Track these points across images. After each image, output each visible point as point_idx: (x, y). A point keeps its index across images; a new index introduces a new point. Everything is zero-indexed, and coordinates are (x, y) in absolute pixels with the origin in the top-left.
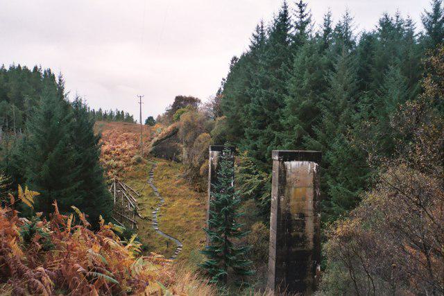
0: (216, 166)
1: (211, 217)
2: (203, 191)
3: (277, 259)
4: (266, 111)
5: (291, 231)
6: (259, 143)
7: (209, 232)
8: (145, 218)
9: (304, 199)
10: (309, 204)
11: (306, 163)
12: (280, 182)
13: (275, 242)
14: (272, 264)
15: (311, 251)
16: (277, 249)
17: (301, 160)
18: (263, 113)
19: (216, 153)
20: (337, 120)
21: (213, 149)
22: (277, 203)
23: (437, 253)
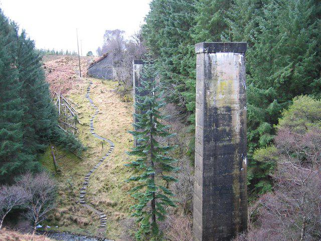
0: (139, 78)
1: (137, 121)
2: (129, 101)
3: (204, 155)
4: (179, 31)
5: (217, 126)
6: (174, 58)
7: (136, 134)
8: (84, 124)
9: (230, 92)
10: (236, 96)
11: (231, 54)
12: (205, 75)
13: (202, 138)
14: (199, 159)
15: (237, 144)
16: (204, 144)
17: (227, 51)
18: (176, 34)
19: (138, 66)
20: (243, 31)
21: (136, 62)
22: (203, 98)
23: (303, 239)
